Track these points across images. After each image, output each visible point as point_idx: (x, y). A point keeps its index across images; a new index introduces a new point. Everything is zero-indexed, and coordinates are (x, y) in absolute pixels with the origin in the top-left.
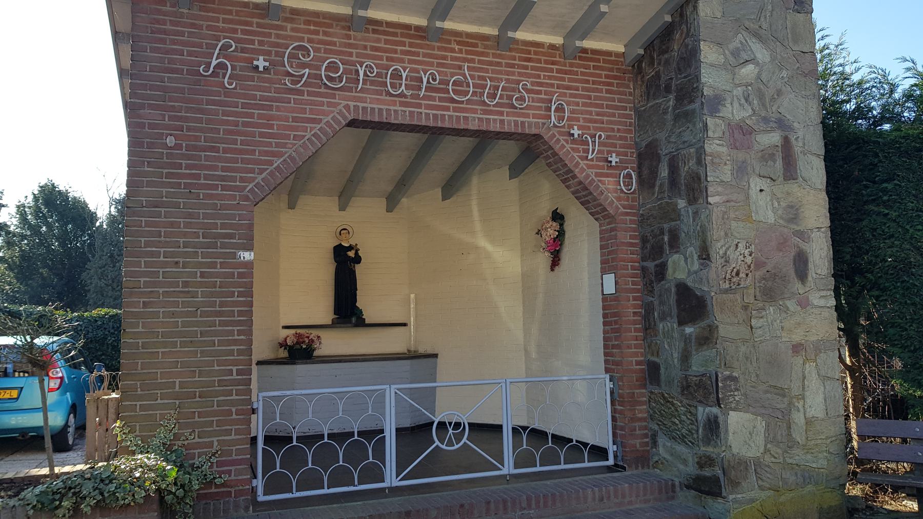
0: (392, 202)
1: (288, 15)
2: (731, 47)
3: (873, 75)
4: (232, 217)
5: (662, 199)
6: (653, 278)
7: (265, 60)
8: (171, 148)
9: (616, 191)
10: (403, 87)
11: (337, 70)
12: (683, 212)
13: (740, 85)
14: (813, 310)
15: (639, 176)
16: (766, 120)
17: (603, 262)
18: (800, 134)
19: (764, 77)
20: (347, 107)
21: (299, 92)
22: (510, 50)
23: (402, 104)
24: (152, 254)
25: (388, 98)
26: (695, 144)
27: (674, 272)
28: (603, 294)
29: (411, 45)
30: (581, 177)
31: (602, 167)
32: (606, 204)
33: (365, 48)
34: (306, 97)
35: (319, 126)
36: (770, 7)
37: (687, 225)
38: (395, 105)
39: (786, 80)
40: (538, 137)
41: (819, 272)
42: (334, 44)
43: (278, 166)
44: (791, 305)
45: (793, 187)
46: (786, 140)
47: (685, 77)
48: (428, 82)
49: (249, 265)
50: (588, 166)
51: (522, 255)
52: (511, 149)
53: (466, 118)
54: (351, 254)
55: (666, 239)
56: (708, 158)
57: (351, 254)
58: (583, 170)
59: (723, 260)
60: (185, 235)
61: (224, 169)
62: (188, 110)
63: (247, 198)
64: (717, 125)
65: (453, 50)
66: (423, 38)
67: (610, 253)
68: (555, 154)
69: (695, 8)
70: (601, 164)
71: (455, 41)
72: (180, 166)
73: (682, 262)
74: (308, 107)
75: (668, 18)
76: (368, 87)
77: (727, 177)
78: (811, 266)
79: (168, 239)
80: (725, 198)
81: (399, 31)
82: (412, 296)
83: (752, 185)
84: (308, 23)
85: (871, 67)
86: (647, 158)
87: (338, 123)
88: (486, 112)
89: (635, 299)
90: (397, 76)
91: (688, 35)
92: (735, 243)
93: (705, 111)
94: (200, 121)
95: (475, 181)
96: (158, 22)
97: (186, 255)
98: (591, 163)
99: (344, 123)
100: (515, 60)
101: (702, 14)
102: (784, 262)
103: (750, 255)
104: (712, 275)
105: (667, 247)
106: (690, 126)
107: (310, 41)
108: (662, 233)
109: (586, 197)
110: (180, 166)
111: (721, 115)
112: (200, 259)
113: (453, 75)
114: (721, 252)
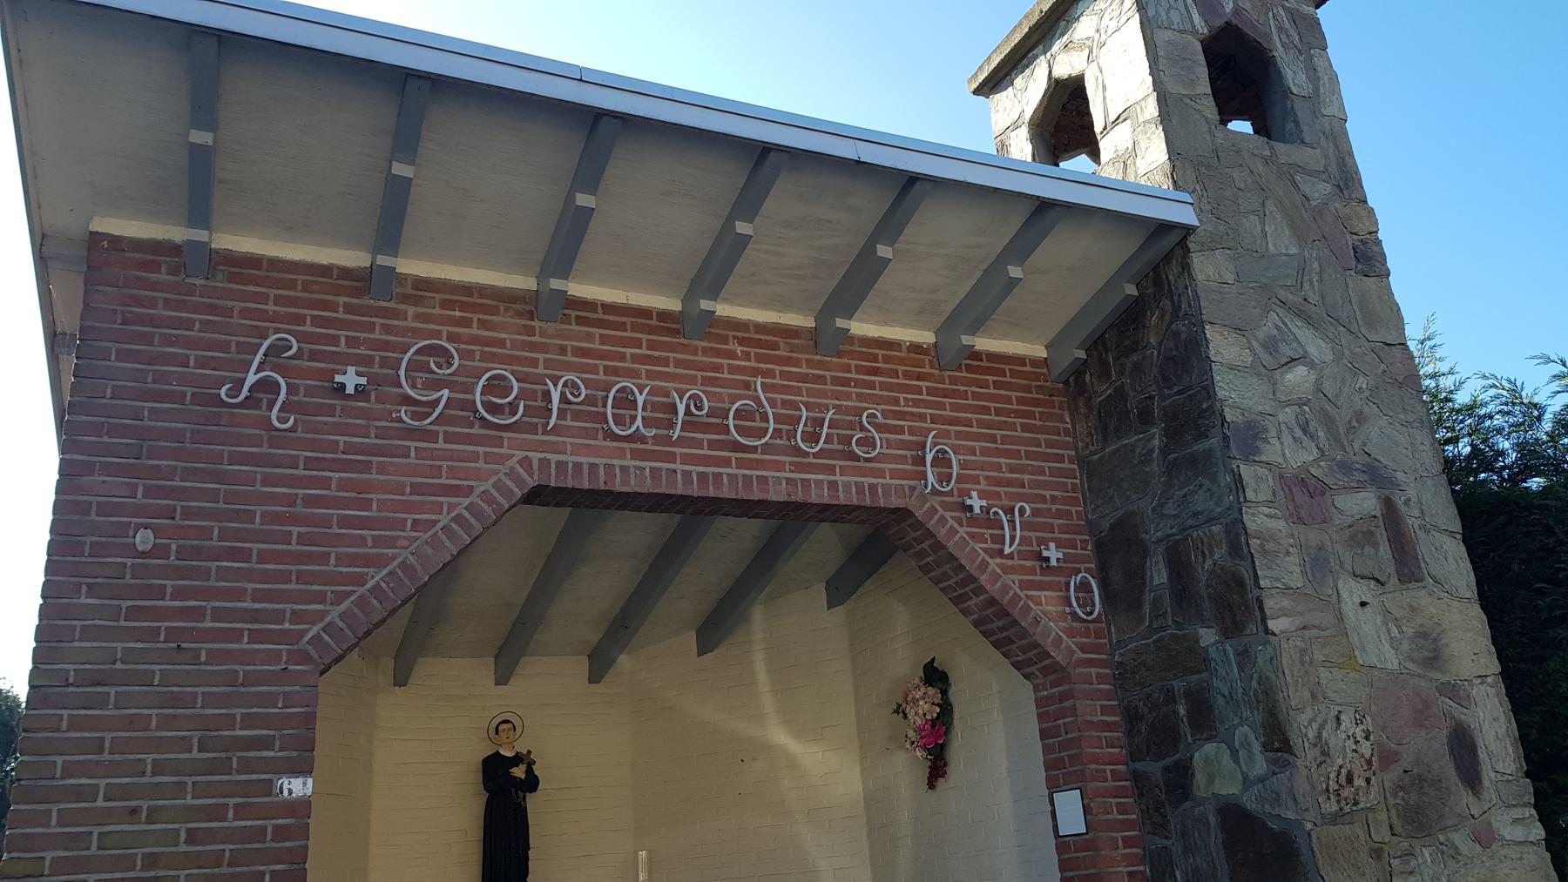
0: (599, 664)
1: (409, 291)
2: (1260, 334)
3: (1493, 392)
4: (270, 700)
5: (1162, 628)
6: (1163, 797)
7: (358, 374)
8: (143, 554)
9: (1062, 616)
10: (639, 422)
11: (507, 391)
12: (1213, 653)
13: (1288, 404)
14: (1506, 851)
15: (1104, 586)
16: (1345, 467)
17: (1049, 766)
18: (1412, 493)
19: (1328, 387)
20: (526, 463)
21: (430, 436)
22: (840, 354)
23: (636, 455)
24: (78, 794)
25: (608, 444)
26: (1221, 515)
27: (1211, 781)
28: (1057, 835)
29: (652, 345)
30: (994, 590)
31: (1032, 571)
32: (1047, 643)
33: (563, 350)
34: (441, 444)
35: (467, 501)
36: (1316, 265)
37: (1226, 679)
38: (623, 457)
39: (1367, 393)
40: (902, 514)
41: (1500, 767)
42: (502, 344)
43: (377, 585)
44: (1461, 839)
45: (1419, 596)
46: (1389, 505)
47: (1179, 392)
48: (688, 412)
49: (301, 808)
50: (1002, 567)
51: (863, 759)
52: (824, 547)
53: (763, 480)
54: (519, 772)
55: (1182, 711)
56: (1254, 542)
57: (519, 772)
58: (995, 577)
59: (1317, 751)
60: (159, 745)
61: (258, 596)
62: (188, 474)
63: (304, 657)
64: (1258, 479)
65: (732, 355)
66: (675, 333)
67: (1063, 746)
68: (938, 546)
69: (1186, 267)
70: (1028, 563)
71: (735, 337)
72: (160, 593)
73: (1226, 759)
74: (445, 464)
75: (1131, 290)
76: (568, 422)
77: (1296, 580)
78: (1482, 755)
79: (117, 757)
80: (1298, 622)
81: (628, 320)
82: (643, 854)
83: (1345, 595)
84: (446, 304)
85: (1484, 377)
86: (1116, 553)
87: (507, 493)
88: (800, 468)
89: (1128, 842)
90: (625, 401)
91: (1175, 316)
92: (1333, 713)
93: (1234, 452)
94: (214, 496)
95: (758, 614)
96: (138, 302)
97: (157, 791)
98: (1009, 562)
99: (518, 493)
100: (849, 371)
101: (1199, 276)
102: (1430, 747)
103: (1367, 738)
104: (1301, 784)
105: (1185, 728)
106: (1206, 482)
107: (452, 338)
108: (1171, 698)
109: (1004, 631)
110: (160, 593)
111: (1264, 458)
112: (189, 801)
113: (733, 399)
114: (1311, 735)
